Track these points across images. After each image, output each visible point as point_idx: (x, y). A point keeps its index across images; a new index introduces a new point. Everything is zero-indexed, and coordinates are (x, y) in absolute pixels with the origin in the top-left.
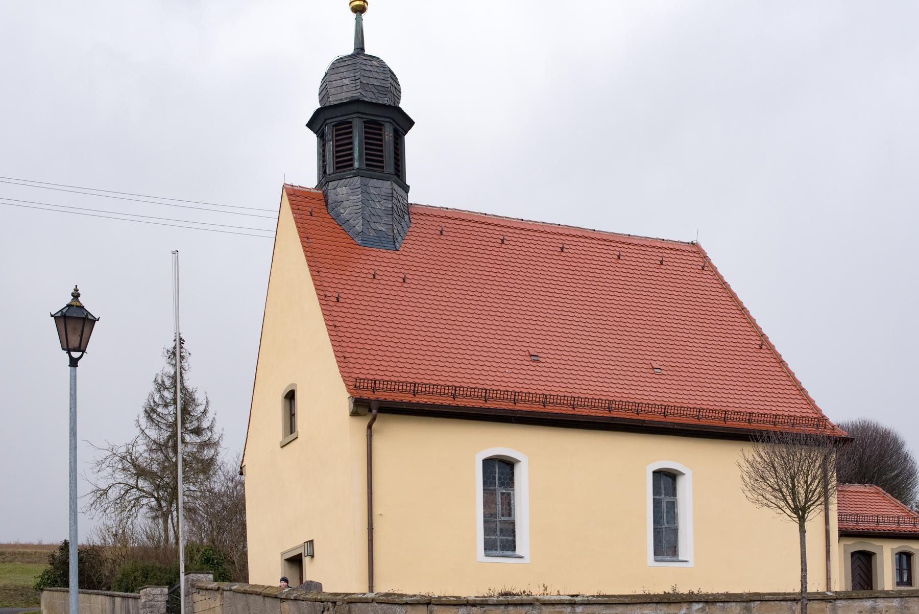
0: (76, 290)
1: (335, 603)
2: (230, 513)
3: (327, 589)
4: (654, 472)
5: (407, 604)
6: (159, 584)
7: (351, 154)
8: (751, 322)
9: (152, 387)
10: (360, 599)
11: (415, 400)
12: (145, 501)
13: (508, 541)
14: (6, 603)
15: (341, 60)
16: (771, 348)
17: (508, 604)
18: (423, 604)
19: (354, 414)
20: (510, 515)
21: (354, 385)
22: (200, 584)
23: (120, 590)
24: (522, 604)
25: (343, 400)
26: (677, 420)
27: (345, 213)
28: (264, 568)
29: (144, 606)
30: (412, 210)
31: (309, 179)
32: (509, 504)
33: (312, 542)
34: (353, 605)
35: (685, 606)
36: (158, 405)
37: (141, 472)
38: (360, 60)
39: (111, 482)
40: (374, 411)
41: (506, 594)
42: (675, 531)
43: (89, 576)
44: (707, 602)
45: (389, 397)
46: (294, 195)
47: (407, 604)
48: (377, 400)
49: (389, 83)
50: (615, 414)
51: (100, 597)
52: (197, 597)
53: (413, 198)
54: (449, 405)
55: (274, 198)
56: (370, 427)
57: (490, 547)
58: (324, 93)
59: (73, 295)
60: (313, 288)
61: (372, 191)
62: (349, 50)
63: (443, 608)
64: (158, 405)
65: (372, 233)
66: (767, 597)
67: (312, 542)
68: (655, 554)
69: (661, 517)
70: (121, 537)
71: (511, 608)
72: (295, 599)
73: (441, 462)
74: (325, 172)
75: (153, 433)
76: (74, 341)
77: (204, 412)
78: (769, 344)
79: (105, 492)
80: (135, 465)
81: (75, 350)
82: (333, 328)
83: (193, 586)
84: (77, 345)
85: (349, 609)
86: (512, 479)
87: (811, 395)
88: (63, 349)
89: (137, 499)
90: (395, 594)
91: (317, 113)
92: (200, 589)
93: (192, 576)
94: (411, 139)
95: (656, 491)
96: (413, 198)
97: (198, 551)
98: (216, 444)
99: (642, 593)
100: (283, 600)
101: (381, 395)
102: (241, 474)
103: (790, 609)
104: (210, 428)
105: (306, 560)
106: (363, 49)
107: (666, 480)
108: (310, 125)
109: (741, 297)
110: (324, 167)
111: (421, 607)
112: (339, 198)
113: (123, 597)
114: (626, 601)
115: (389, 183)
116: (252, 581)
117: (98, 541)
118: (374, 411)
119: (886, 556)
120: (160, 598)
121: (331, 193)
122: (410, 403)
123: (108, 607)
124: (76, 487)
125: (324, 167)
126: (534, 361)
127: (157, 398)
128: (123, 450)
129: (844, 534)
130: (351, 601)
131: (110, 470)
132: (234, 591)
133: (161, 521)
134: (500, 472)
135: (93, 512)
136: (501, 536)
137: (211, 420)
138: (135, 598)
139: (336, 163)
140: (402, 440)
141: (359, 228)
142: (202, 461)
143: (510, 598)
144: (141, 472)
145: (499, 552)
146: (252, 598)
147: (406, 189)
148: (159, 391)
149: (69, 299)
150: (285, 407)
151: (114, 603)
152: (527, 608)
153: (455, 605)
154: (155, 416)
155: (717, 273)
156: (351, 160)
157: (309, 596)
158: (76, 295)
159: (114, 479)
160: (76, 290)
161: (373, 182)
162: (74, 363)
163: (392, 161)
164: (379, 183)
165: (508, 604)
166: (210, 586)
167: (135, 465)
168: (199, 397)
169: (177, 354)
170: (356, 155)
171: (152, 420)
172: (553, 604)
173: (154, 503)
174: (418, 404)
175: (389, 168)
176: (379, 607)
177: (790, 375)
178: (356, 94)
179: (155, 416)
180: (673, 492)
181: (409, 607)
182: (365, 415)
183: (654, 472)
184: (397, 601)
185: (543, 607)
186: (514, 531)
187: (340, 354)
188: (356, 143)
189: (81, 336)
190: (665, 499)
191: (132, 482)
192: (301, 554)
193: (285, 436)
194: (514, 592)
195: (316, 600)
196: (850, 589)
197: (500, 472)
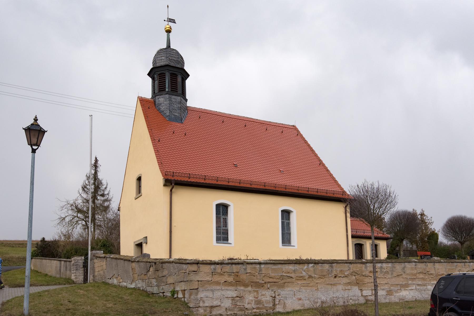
0: (36, 117)
1: (155, 263)
2: (114, 227)
3: (152, 257)
4: (282, 211)
5: (188, 263)
6: (81, 256)
7: (165, 86)
8: (316, 155)
9: (85, 178)
10: (167, 261)
11: (189, 180)
12: (80, 222)
13: (225, 237)
14: (18, 264)
15: (161, 50)
16: (324, 165)
17: (232, 264)
18: (195, 264)
19: (165, 185)
20: (226, 227)
21: (165, 174)
22: (97, 255)
23: (65, 258)
24: (238, 264)
25: (160, 180)
26: (290, 191)
27: (162, 108)
28: (127, 249)
29: (73, 265)
30: (188, 108)
31: (148, 95)
32: (226, 222)
33: (146, 237)
34: (164, 264)
35: (306, 265)
36: (87, 185)
37: (79, 211)
38: (168, 50)
39: (67, 214)
40: (173, 184)
41: (231, 259)
42: (290, 234)
43: (53, 252)
44: (315, 263)
45: (179, 179)
46: (142, 101)
47: (188, 263)
48: (174, 180)
49: (180, 60)
50: (267, 188)
51: (55, 261)
52: (96, 261)
53: (189, 104)
54: (203, 183)
55: (134, 102)
56: (171, 191)
57: (218, 240)
58: (154, 62)
59: (34, 119)
60: (149, 136)
61: (173, 100)
62: (165, 47)
63: (204, 265)
64: (87, 185)
65: (173, 116)
66: (339, 262)
67: (146, 237)
68: (282, 243)
69: (284, 228)
70: (68, 236)
71: (234, 265)
72: (138, 262)
73: (198, 206)
74: (154, 93)
75: (85, 196)
76: (34, 141)
77: (106, 188)
78: (323, 163)
79: (64, 219)
80: (76, 207)
81: (34, 145)
82: (157, 152)
83: (94, 256)
84: (35, 143)
85: (162, 266)
86: (227, 212)
87: (339, 183)
88: (29, 145)
89: (77, 221)
90: (18, 297)
91: (152, 70)
92: (97, 257)
93: (94, 252)
94: (188, 82)
95: (282, 218)
96: (189, 104)
97: (100, 241)
98: (110, 200)
99: (286, 259)
100: (132, 262)
101: (176, 178)
102: (119, 210)
103: (349, 267)
104: (108, 194)
105: (144, 245)
106: (170, 46)
107: (286, 214)
108: (149, 74)
109: (312, 146)
110: (154, 91)
111: (194, 265)
112: (160, 102)
113: (65, 261)
114: (282, 262)
115: (180, 97)
116: (122, 253)
117: (57, 238)
118: (173, 184)
119: (368, 245)
120: (80, 261)
121: (157, 101)
122: (187, 181)
123: (58, 265)
124: (32, 209)
125: (154, 91)
126: (235, 167)
127: (87, 182)
128: (72, 202)
129: (353, 237)
130: (163, 262)
131: (66, 210)
132: (112, 258)
133: (87, 230)
134: (222, 209)
135: (59, 226)
136: (222, 235)
137: (108, 190)
138: (70, 261)
139: (159, 89)
140: (184, 197)
141: (168, 114)
142: (104, 207)
143: (233, 261)
144: (79, 211)
145: (222, 242)
146: (119, 261)
147: (186, 100)
148: (88, 179)
149: (32, 121)
150: (137, 183)
151: (61, 264)
152: (240, 266)
153: (210, 264)
154: (86, 189)
155: (303, 137)
156: (165, 88)
157: (144, 260)
158: (36, 120)
159: (68, 213)
160: (36, 117)
161: (173, 97)
162: (34, 151)
163: (181, 89)
164: (176, 97)
165: (232, 264)
166: (101, 256)
167: (76, 207)
168: (104, 182)
169: (95, 166)
170: (167, 86)
171: (85, 191)
172: (252, 264)
173: (84, 223)
174: (190, 182)
175: (180, 91)
176: (176, 265)
177: (331, 175)
178: (167, 63)
179: (86, 189)
180: (289, 219)
181: (189, 265)
182: (169, 186)
183: (282, 211)
184: (184, 262)
185: (247, 265)
186: (228, 233)
187: (159, 162)
188: (167, 81)
189: (38, 138)
190: (286, 222)
191: (75, 215)
192: (142, 243)
193: (137, 195)
194: (234, 258)
195: (147, 262)
196: (355, 259)
197: (222, 209)
